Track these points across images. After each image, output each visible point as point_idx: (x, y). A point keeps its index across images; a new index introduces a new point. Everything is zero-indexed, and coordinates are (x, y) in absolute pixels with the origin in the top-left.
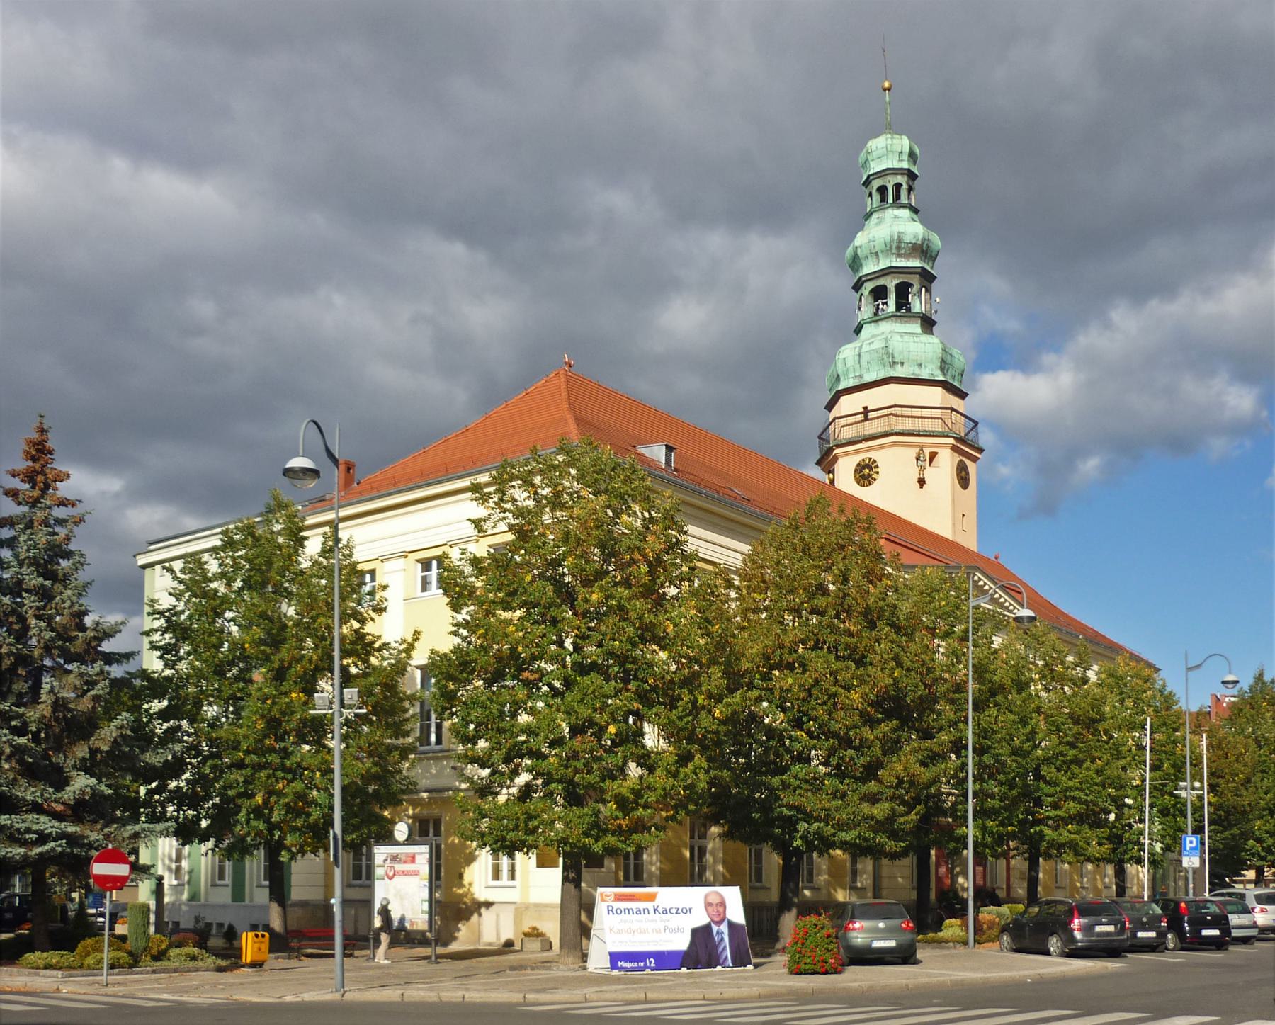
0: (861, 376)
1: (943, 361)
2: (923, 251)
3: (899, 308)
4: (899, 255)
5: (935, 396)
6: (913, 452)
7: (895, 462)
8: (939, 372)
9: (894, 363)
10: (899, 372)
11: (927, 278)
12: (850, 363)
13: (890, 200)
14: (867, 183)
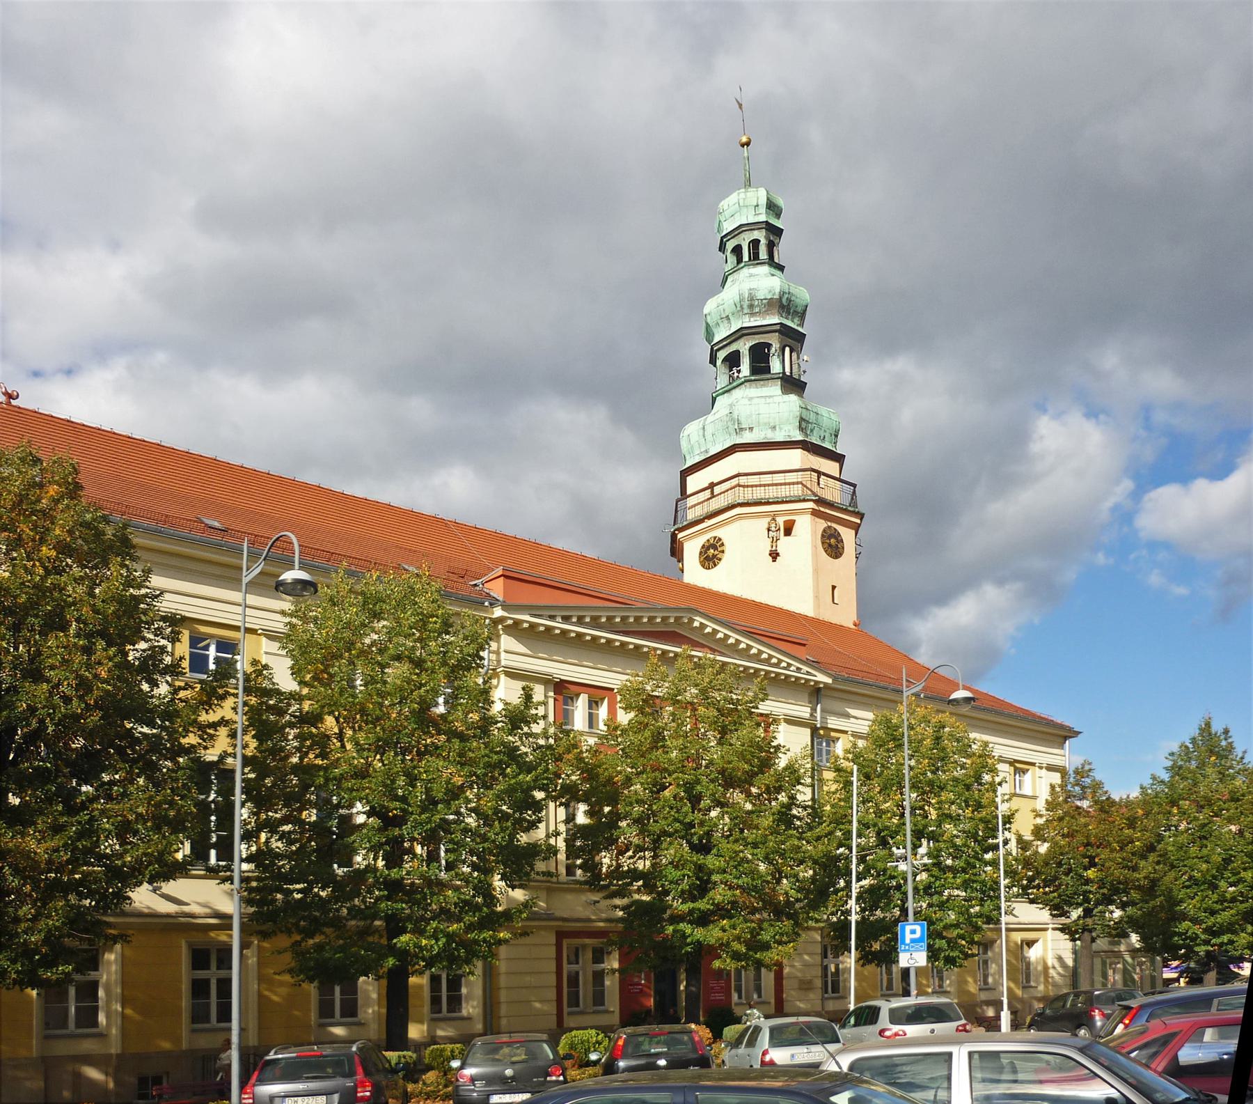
0: (707, 451)
1: (802, 420)
3: (754, 371)
4: (752, 314)
5: (796, 458)
6: (764, 522)
7: (743, 537)
9: (741, 429)
10: (748, 438)
11: (793, 339)
12: (694, 438)
13: (746, 258)
14: (722, 248)
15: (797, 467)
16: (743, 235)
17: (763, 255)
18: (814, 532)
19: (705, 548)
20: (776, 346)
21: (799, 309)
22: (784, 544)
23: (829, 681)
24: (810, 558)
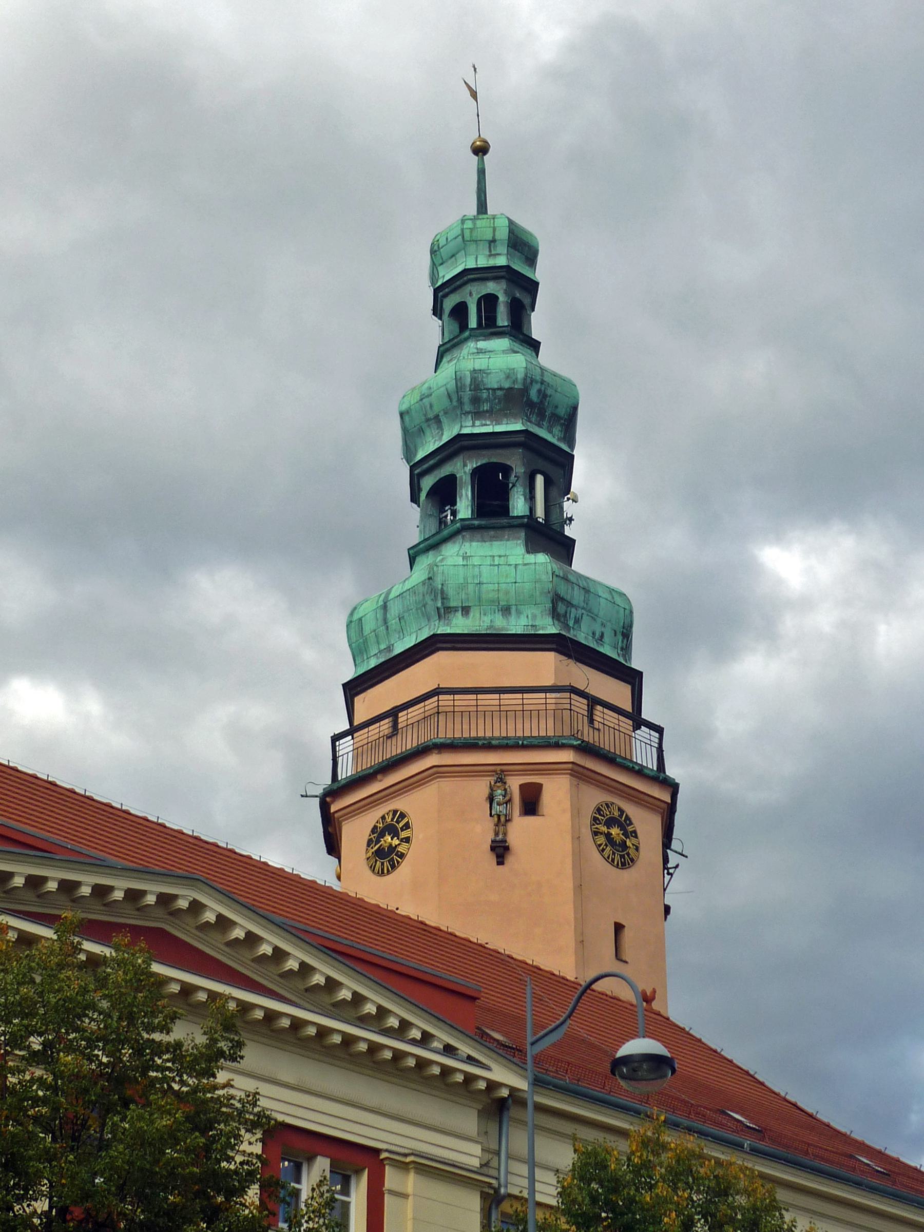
0: (389, 649)
2: (531, 404)
3: (482, 508)
4: (478, 415)
5: (545, 667)
6: (480, 787)
8: (549, 620)
10: (459, 625)
13: (473, 323)
15: (549, 682)
16: (468, 288)
17: (503, 320)
18: (576, 812)
19: (378, 833)
20: (519, 469)
21: (562, 412)
22: (521, 830)
23: (522, 1084)
24: (569, 861)
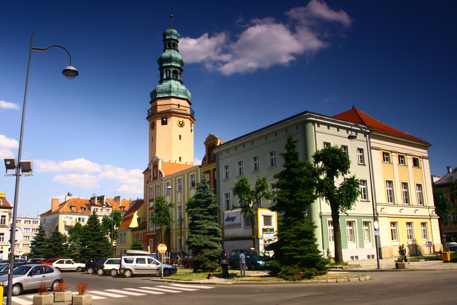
5: (185, 103)
